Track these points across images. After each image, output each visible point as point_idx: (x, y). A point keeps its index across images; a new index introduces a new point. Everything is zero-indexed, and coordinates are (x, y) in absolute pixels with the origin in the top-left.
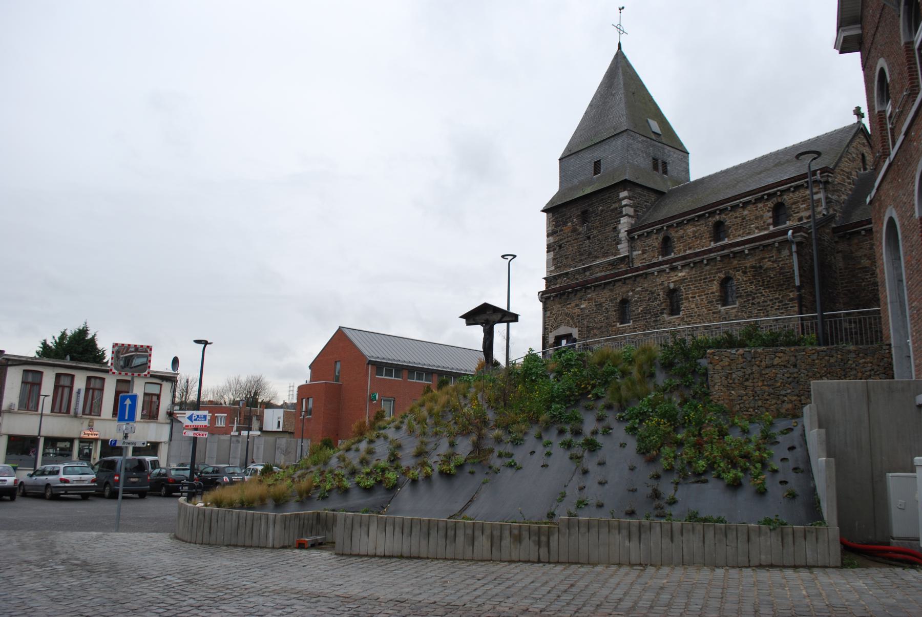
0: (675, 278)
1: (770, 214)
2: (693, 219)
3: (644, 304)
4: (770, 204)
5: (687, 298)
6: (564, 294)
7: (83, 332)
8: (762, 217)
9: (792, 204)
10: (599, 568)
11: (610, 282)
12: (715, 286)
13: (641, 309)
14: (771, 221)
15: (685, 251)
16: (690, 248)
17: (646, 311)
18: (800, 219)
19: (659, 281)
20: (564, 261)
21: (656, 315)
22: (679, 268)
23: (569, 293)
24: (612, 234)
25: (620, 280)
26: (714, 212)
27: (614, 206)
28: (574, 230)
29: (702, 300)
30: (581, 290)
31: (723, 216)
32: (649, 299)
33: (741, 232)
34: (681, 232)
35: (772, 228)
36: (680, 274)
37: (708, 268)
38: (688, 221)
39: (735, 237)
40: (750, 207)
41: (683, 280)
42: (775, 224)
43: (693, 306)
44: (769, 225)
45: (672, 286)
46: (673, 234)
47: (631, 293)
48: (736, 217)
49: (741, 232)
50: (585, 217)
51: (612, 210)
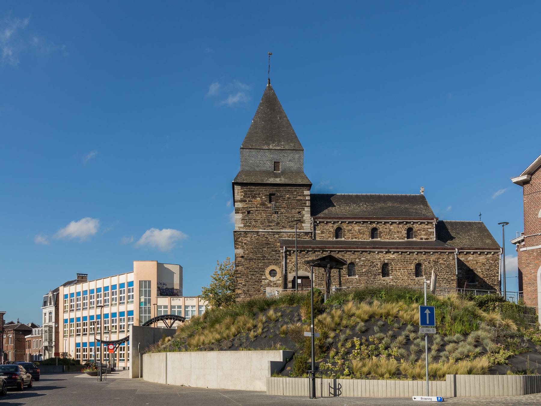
0: (388, 258)
1: (406, 232)
2: (360, 222)
3: (367, 268)
4: (406, 227)
5: (396, 270)
6: (304, 251)
7: (271, 362)
8: (401, 232)
9: (419, 230)
10: (294, 357)
11: (343, 251)
12: (413, 267)
13: (364, 270)
14: (406, 235)
15: (352, 239)
16: (356, 238)
17: (368, 272)
18: (422, 239)
19: (377, 257)
20: (253, 223)
21: (375, 275)
22: (392, 252)
23: (308, 251)
24: (297, 215)
25: (351, 251)
26: (374, 222)
27: (299, 198)
28: (263, 204)
29: (404, 272)
30: (319, 251)
31: (378, 225)
32: (371, 266)
33: (389, 237)
34: (350, 228)
35: (406, 239)
36: (391, 256)
37: (408, 256)
38: (356, 222)
39: (385, 238)
40: (394, 225)
41: (393, 260)
42: (408, 238)
43: (399, 274)
44: (404, 237)
45: (386, 261)
46: (344, 226)
47: (357, 260)
48: (386, 228)
49: (389, 237)
50: (271, 197)
51: (298, 200)
